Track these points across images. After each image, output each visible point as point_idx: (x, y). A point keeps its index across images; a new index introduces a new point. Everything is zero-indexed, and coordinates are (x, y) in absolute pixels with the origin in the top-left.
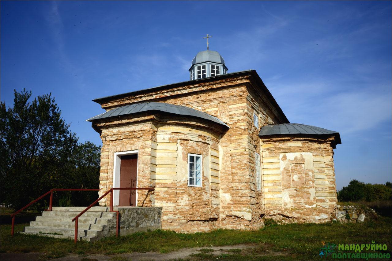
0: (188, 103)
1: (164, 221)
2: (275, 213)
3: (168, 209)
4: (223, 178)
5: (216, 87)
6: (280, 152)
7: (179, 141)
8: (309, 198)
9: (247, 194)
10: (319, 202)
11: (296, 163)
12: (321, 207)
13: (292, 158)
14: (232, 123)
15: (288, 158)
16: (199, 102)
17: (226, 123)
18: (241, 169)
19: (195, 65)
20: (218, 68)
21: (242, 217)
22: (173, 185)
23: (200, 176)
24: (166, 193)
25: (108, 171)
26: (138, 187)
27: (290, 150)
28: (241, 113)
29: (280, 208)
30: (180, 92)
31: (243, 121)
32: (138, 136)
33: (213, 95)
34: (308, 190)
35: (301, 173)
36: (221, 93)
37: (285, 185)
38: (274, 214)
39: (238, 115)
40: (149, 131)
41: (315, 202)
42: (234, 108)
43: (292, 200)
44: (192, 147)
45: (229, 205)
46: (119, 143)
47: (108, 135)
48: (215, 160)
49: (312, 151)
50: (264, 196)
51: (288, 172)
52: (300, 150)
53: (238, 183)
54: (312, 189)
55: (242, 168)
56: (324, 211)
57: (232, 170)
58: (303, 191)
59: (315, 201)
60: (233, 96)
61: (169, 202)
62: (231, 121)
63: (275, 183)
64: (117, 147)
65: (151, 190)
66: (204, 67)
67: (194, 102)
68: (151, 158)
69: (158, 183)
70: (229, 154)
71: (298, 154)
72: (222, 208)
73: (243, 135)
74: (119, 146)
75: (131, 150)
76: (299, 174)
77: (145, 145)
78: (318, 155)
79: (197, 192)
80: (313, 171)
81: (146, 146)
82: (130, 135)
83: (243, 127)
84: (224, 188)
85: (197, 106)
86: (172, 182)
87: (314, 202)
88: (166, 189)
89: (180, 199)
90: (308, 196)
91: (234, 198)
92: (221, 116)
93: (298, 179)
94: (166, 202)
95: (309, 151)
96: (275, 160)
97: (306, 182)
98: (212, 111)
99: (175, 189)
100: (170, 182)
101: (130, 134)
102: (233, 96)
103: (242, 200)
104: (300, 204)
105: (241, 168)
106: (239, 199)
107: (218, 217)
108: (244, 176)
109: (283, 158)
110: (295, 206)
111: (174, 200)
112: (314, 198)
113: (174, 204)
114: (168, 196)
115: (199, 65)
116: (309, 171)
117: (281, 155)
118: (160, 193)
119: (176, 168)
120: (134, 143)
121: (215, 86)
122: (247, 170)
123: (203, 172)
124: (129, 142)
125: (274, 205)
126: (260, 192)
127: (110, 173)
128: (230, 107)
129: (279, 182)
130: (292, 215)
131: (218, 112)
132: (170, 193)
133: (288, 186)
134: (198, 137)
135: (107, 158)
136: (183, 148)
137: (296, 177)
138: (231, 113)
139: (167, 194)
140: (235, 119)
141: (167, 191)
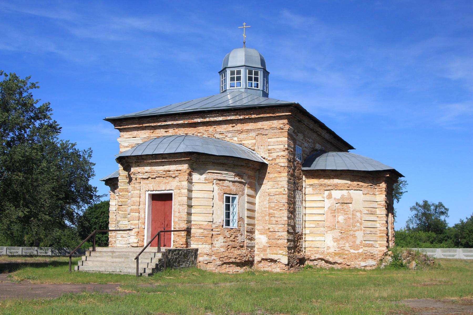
0: (221, 132)
1: (200, 262)
2: (317, 258)
3: (203, 250)
4: (259, 219)
5: (254, 117)
6: (325, 189)
7: (215, 181)
8: (354, 242)
9: (284, 237)
10: (366, 247)
11: (343, 202)
12: (368, 252)
13: (339, 197)
14: (271, 159)
15: (333, 196)
16: (235, 131)
17: (264, 158)
18: (279, 210)
19: (227, 69)
20: (256, 73)
21: (278, 261)
22: (209, 227)
23: (236, 217)
24: (202, 234)
25: (139, 210)
26: (174, 228)
27: (336, 187)
28: (281, 148)
29: (322, 252)
30: (212, 119)
31: (282, 157)
32: (174, 176)
33: (250, 126)
34: (354, 233)
35: (348, 214)
36: (260, 125)
37: (328, 226)
38: (315, 258)
39: (278, 150)
40: (186, 172)
41: (362, 247)
42: (274, 142)
43: (335, 244)
44: (228, 186)
45: (265, 247)
46: (152, 182)
47: (139, 173)
48: (251, 207)
49: (362, 189)
50: (305, 238)
51: (332, 212)
52: (348, 188)
53: (275, 224)
54: (359, 231)
55: (280, 209)
56: (372, 257)
57: (269, 211)
58: (349, 234)
59: (362, 245)
60: (273, 129)
61: (205, 243)
62: (269, 156)
63: (318, 224)
64: (149, 185)
65: (188, 231)
66: (239, 72)
67: (229, 132)
68: (188, 201)
69: (194, 225)
70: (266, 192)
71: (345, 192)
72: (258, 250)
73: (282, 173)
74: (151, 185)
75: (165, 190)
76: (345, 214)
77: (181, 185)
78: (368, 193)
79: (232, 234)
80: (361, 212)
81: (182, 186)
82: (164, 174)
83: (283, 165)
84: (260, 229)
85: (232, 136)
86: (208, 224)
87: (361, 247)
88: (202, 231)
89: (215, 241)
90: (353, 240)
91: (270, 240)
92: (259, 150)
93: (344, 220)
94: (201, 243)
95: (358, 189)
96: (320, 198)
97: (352, 224)
98: (250, 144)
99: (210, 230)
100: (206, 223)
101: (164, 173)
102: (273, 129)
103: (279, 243)
104: (345, 248)
105: (279, 209)
106: (276, 241)
107: (253, 261)
108: (282, 218)
109: (328, 196)
110: (338, 251)
111: (210, 242)
112: (360, 242)
113: (209, 246)
114: (204, 237)
115: (232, 69)
116: (356, 212)
117: (327, 193)
118: (195, 234)
119: (212, 209)
120: (169, 182)
121: (253, 116)
122: (285, 211)
123: (239, 213)
124: (163, 181)
125: (315, 249)
126: (300, 233)
127: (142, 213)
128: (269, 140)
129: (322, 223)
130: (335, 260)
131: (256, 145)
132: (206, 234)
133: (332, 228)
134: (234, 177)
135: (138, 197)
136: (218, 188)
137: (341, 218)
138: (270, 147)
139: (202, 235)
140: (274, 155)
141: (203, 233)
